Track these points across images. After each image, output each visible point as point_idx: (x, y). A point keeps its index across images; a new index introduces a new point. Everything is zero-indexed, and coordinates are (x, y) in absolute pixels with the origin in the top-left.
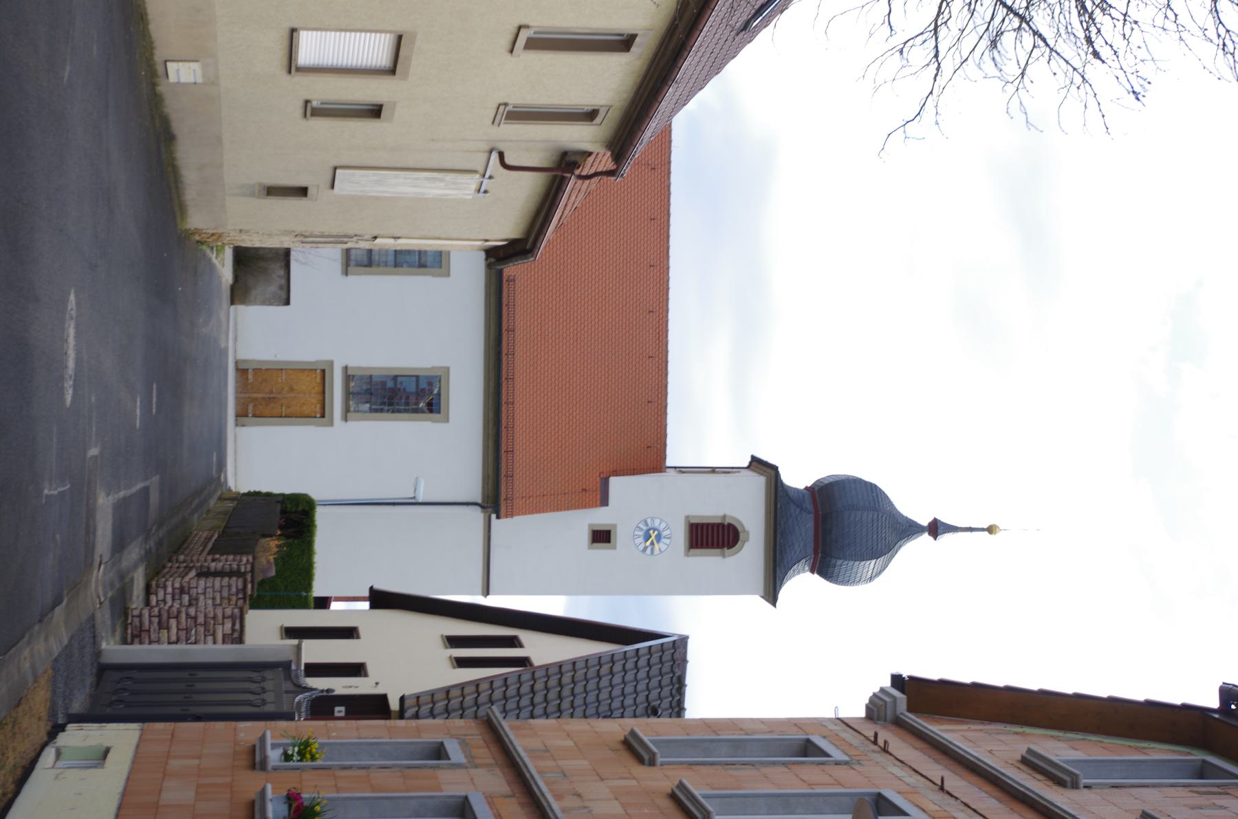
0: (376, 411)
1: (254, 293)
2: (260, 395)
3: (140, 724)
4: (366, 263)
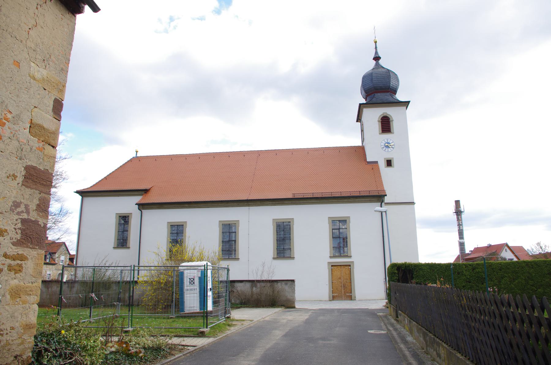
0: (347, 245)
1: (289, 297)
2: (343, 290)
4: (290, 251)
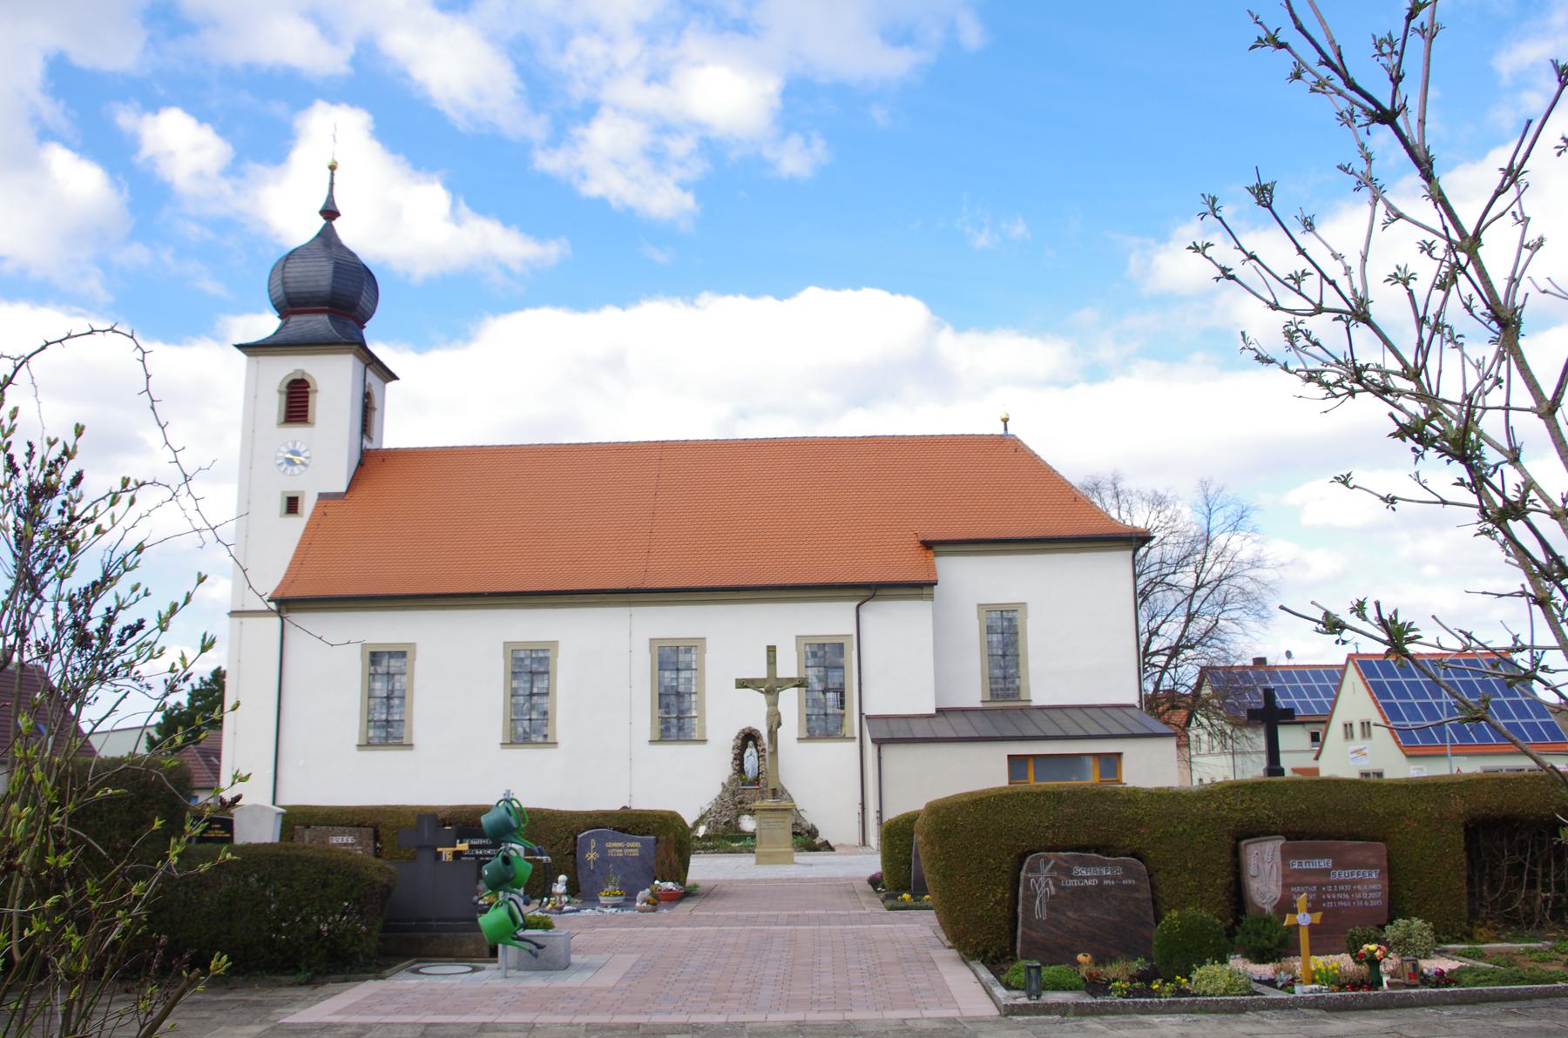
3: (1271, 964)
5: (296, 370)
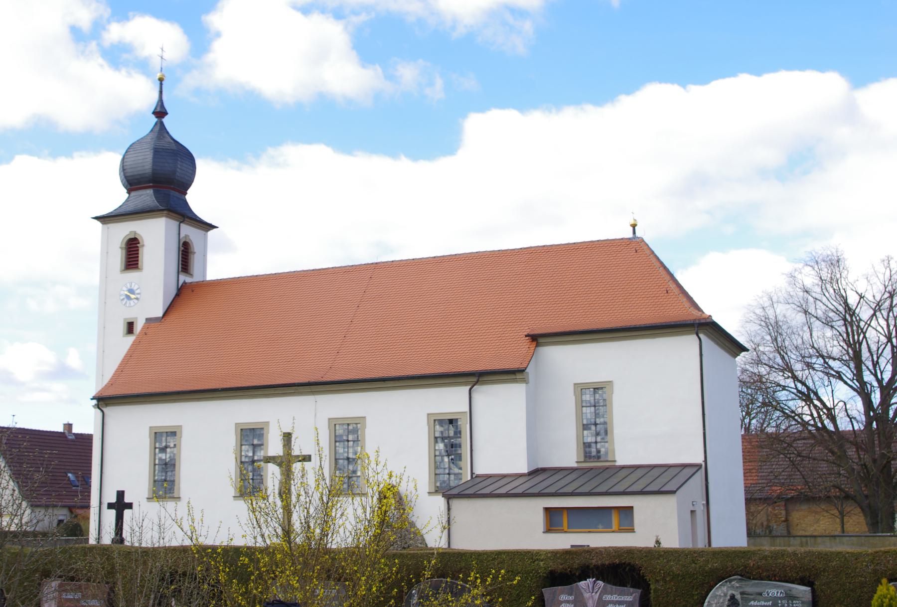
5: (130, 232)
